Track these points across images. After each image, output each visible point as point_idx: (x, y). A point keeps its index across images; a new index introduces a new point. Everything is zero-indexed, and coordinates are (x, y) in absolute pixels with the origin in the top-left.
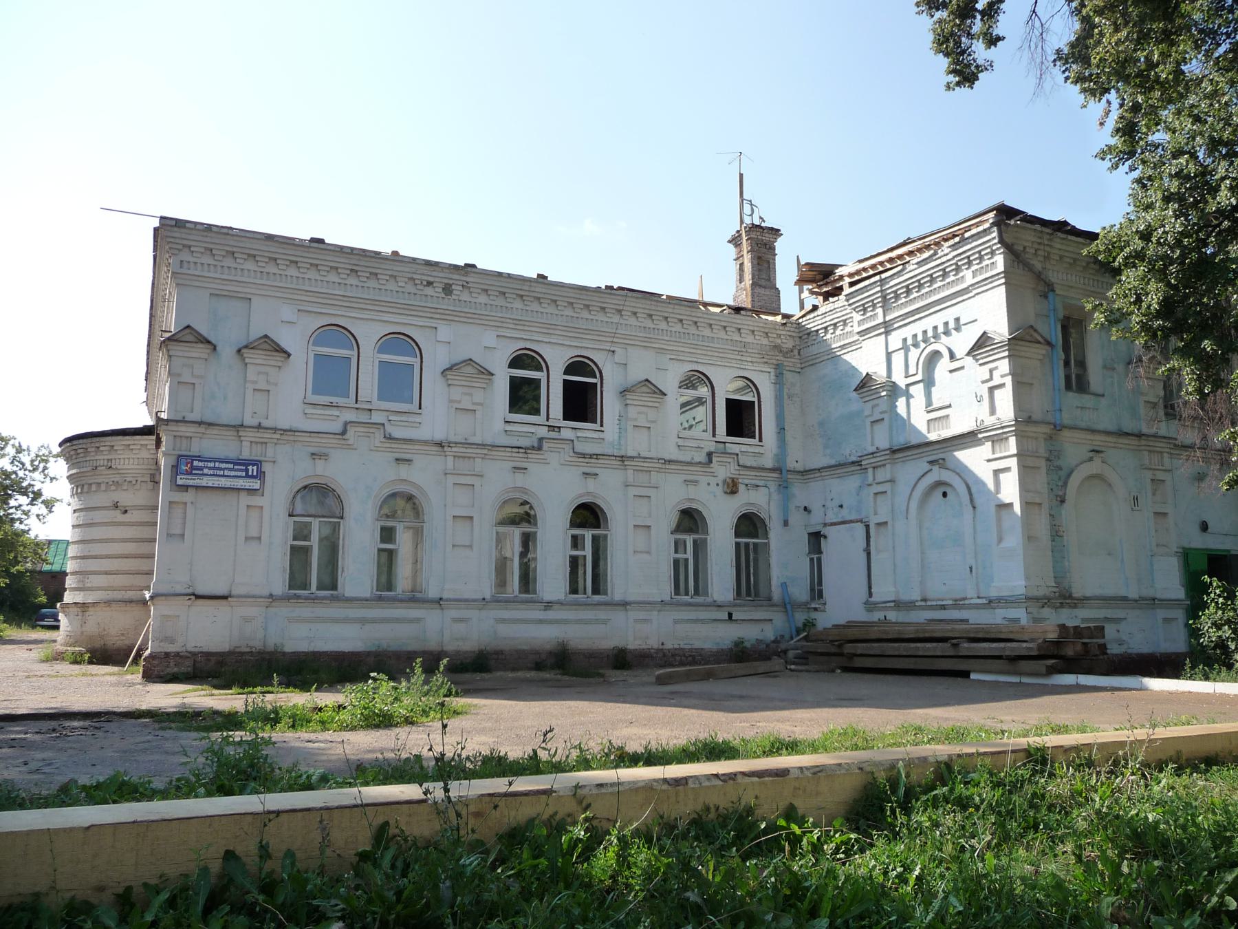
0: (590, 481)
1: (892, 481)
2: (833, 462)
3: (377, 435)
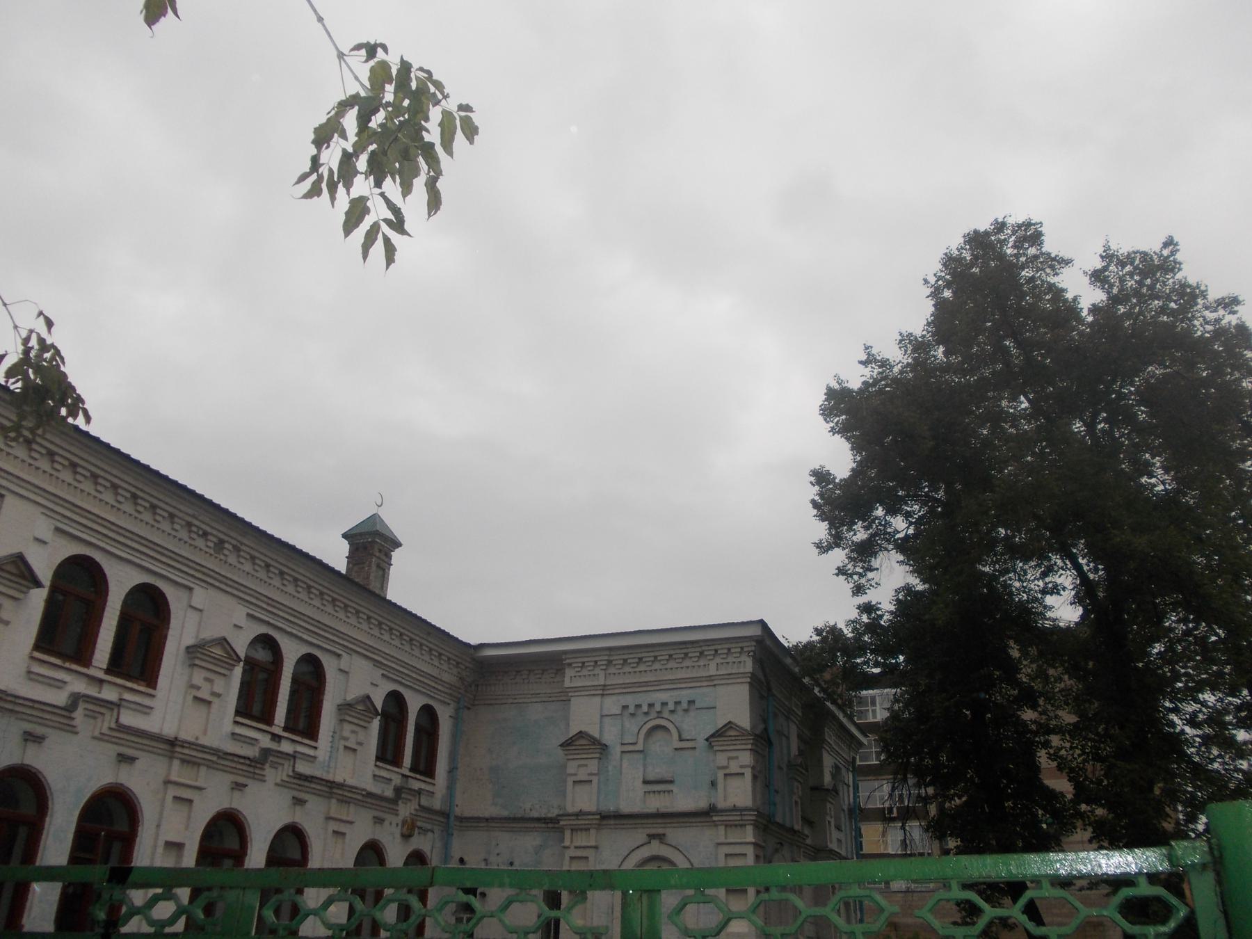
0: (125, 768)
1: (596, 847)
2: (505, 813)
3: (107, 717)
